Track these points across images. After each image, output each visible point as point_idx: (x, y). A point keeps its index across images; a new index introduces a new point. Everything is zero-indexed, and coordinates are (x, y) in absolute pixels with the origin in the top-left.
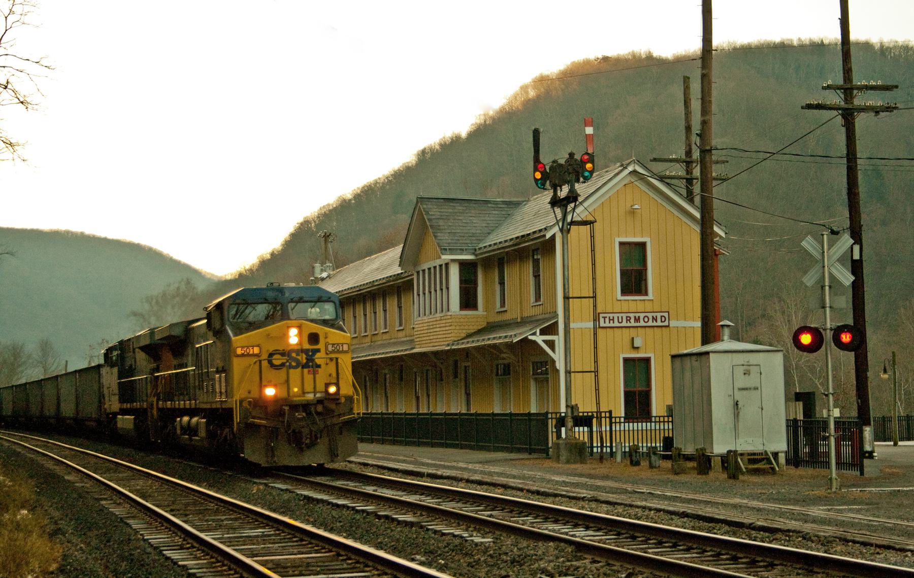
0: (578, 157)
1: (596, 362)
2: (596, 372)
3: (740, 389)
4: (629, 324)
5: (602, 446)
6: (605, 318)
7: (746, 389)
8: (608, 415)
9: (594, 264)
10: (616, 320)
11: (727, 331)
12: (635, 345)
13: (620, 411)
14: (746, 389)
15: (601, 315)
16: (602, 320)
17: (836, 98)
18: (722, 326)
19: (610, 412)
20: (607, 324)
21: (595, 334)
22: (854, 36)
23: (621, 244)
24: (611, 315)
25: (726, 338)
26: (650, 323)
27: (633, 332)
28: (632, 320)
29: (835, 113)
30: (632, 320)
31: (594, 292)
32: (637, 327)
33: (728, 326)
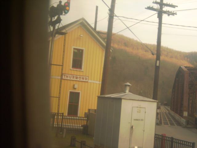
0: (63, 4)
1: (60, 93)
2: (59, 98)
3: (134, 120)
4: (73, 79)
5: (58, 124)
6: (65, 76)
7: (138, 120)
8: (62, 115)
9: (63, 58)
10: (69, 77)
11: (128, 89)
12: (75, 87)
13: (66, 114)
14: (138, 120)
15: (63, 75)
16: (63, 76)
17: (156, 6)
18: (126, 85)
19: (63, 114)
20: (65, 78)
21: (61, 81)
22: (114, 31)
23: (74, 49)
24: (67, 75)
25: (127, 91)
26: (81, 80)
27: (75, 83)
28: (75, 78)
29: (155, 12)
30: (75, 78)
31: (63, 63)
32: (82, 81)
33: (129, 86)
